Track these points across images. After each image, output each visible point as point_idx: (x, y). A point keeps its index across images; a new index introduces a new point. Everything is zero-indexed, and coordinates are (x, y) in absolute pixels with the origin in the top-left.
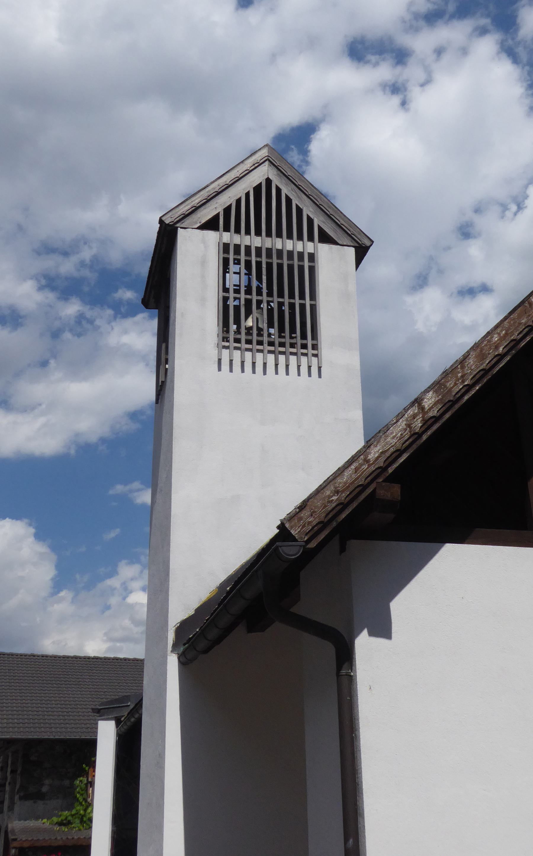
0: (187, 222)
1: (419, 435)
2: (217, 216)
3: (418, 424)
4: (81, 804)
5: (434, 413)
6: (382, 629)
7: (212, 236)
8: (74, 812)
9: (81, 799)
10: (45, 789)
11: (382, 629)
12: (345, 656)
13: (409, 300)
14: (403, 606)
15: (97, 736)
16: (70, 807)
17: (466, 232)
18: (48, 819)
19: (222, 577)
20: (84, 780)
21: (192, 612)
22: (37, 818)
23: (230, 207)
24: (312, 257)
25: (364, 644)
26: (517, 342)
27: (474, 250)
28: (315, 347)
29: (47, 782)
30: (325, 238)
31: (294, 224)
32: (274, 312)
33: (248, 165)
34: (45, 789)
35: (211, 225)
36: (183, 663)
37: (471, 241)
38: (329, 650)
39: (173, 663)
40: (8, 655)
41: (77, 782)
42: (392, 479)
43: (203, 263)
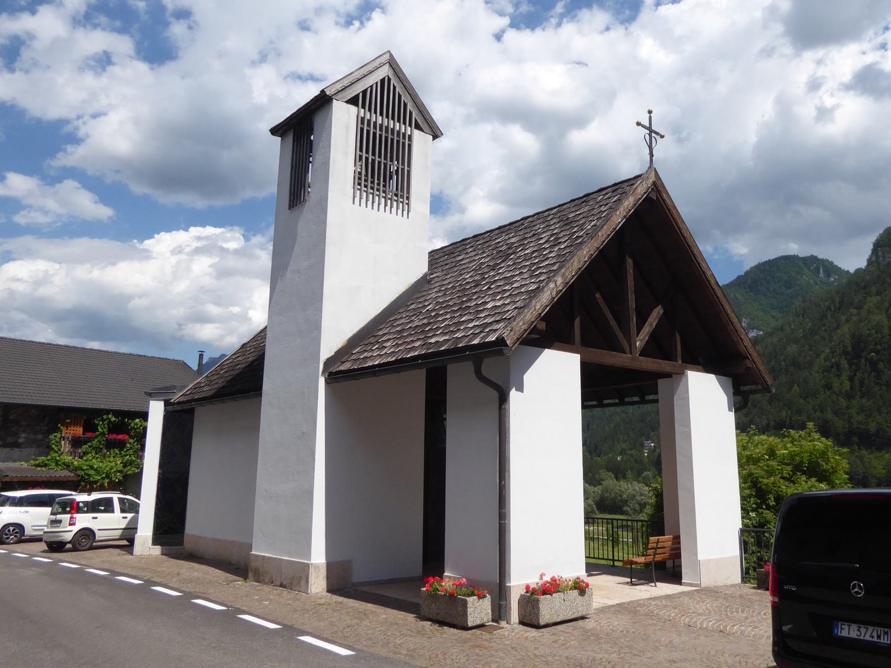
0: (339, 96)
1: (554, 298)
2: (357, 96)
3: (554, 293)
4: (55, 452)
5: (560, 288)
6: (520, 389)
7: (353, 109)
8: (49, 457)
9: (56, 449)
10: (21, 440)
11: (520, 389)
12: (503, 399)
13: (248, 71)
14: (529, 377)
15: (742, 448)
16: (47, 454)
17: (304, 26)
18: (26, 462)
19: (350, 335)
20: (59, 435)
21: (333, 354)
22: (15, 461)
23: (366, 90)
24: (410, 137)
25: (513, 394)
26: (592, 255)
27: (307, 41)
28: (408, 198)
29: (23, 435)
30: (418, 127)
31: (401, 115)
32: (384, 171)
33: (377, 63)
34: (21, 440)
35: (353, 101)
36: (327, 382)
37: (307, 33)
38: (494, 394)
39: (322, 381)
40: (29, 342)
41: (52, 437)
42: (543, 319)
43: (347, 128)
